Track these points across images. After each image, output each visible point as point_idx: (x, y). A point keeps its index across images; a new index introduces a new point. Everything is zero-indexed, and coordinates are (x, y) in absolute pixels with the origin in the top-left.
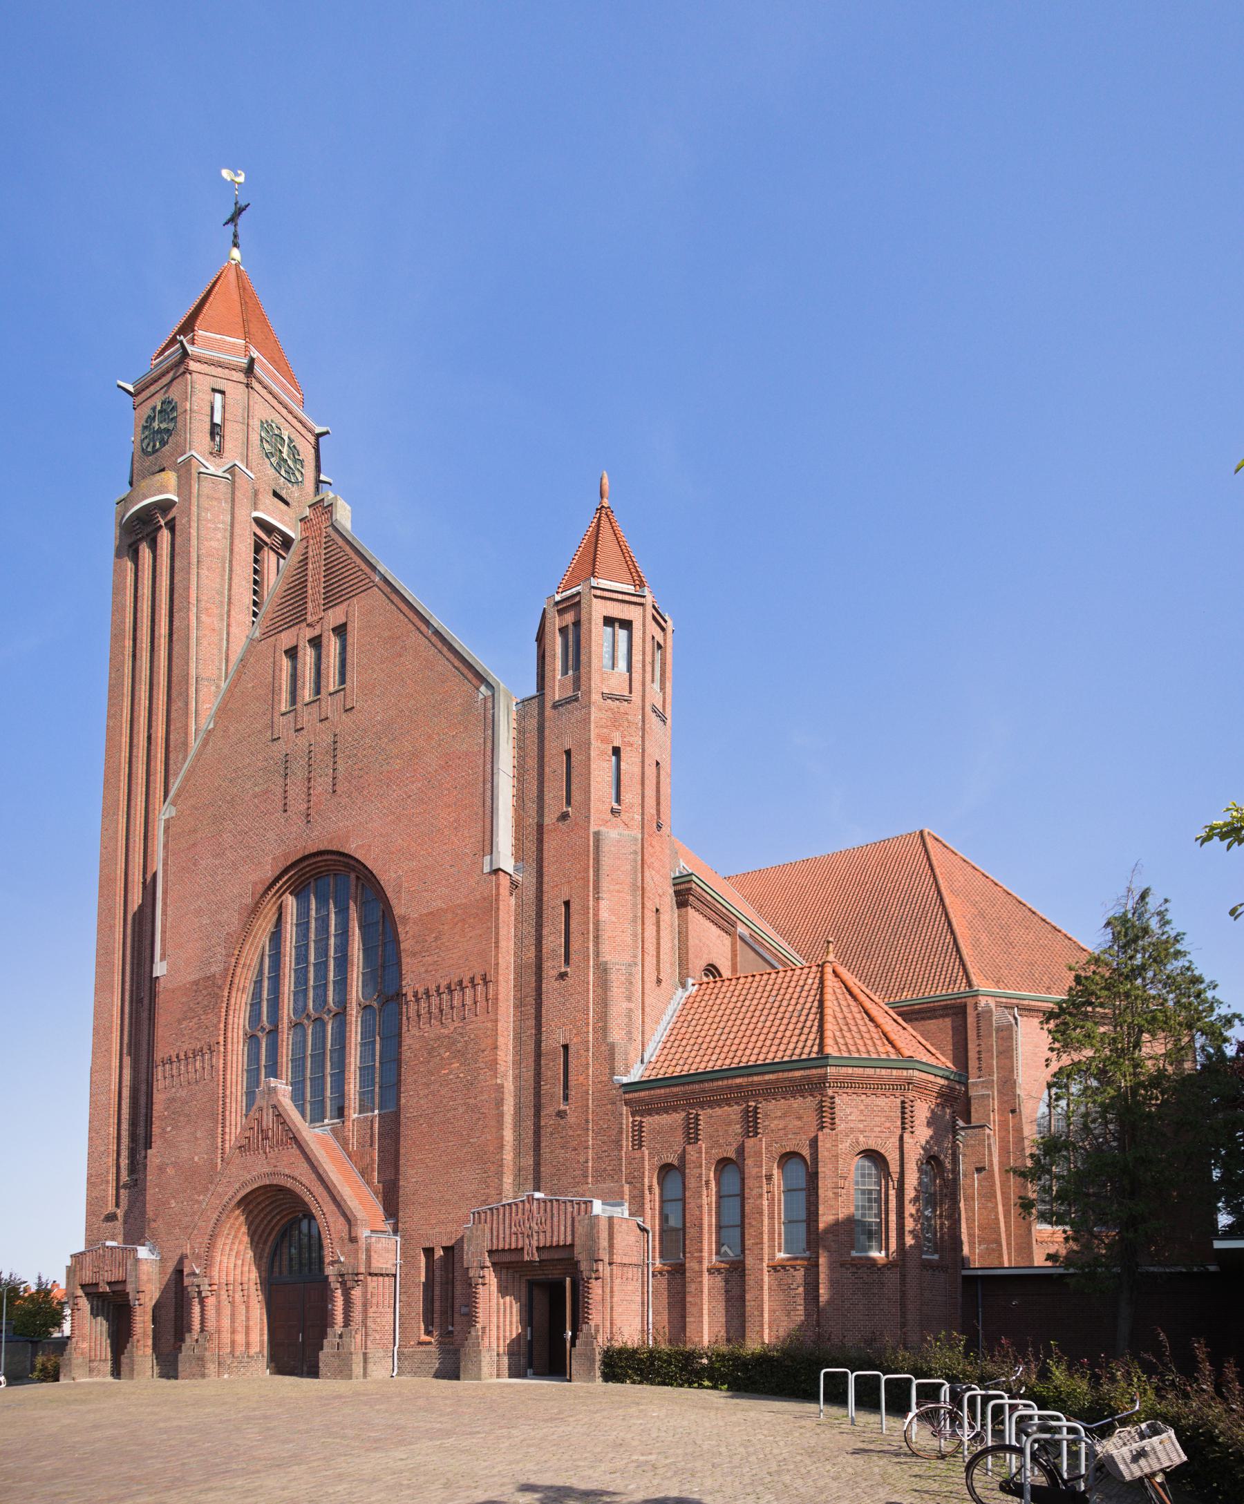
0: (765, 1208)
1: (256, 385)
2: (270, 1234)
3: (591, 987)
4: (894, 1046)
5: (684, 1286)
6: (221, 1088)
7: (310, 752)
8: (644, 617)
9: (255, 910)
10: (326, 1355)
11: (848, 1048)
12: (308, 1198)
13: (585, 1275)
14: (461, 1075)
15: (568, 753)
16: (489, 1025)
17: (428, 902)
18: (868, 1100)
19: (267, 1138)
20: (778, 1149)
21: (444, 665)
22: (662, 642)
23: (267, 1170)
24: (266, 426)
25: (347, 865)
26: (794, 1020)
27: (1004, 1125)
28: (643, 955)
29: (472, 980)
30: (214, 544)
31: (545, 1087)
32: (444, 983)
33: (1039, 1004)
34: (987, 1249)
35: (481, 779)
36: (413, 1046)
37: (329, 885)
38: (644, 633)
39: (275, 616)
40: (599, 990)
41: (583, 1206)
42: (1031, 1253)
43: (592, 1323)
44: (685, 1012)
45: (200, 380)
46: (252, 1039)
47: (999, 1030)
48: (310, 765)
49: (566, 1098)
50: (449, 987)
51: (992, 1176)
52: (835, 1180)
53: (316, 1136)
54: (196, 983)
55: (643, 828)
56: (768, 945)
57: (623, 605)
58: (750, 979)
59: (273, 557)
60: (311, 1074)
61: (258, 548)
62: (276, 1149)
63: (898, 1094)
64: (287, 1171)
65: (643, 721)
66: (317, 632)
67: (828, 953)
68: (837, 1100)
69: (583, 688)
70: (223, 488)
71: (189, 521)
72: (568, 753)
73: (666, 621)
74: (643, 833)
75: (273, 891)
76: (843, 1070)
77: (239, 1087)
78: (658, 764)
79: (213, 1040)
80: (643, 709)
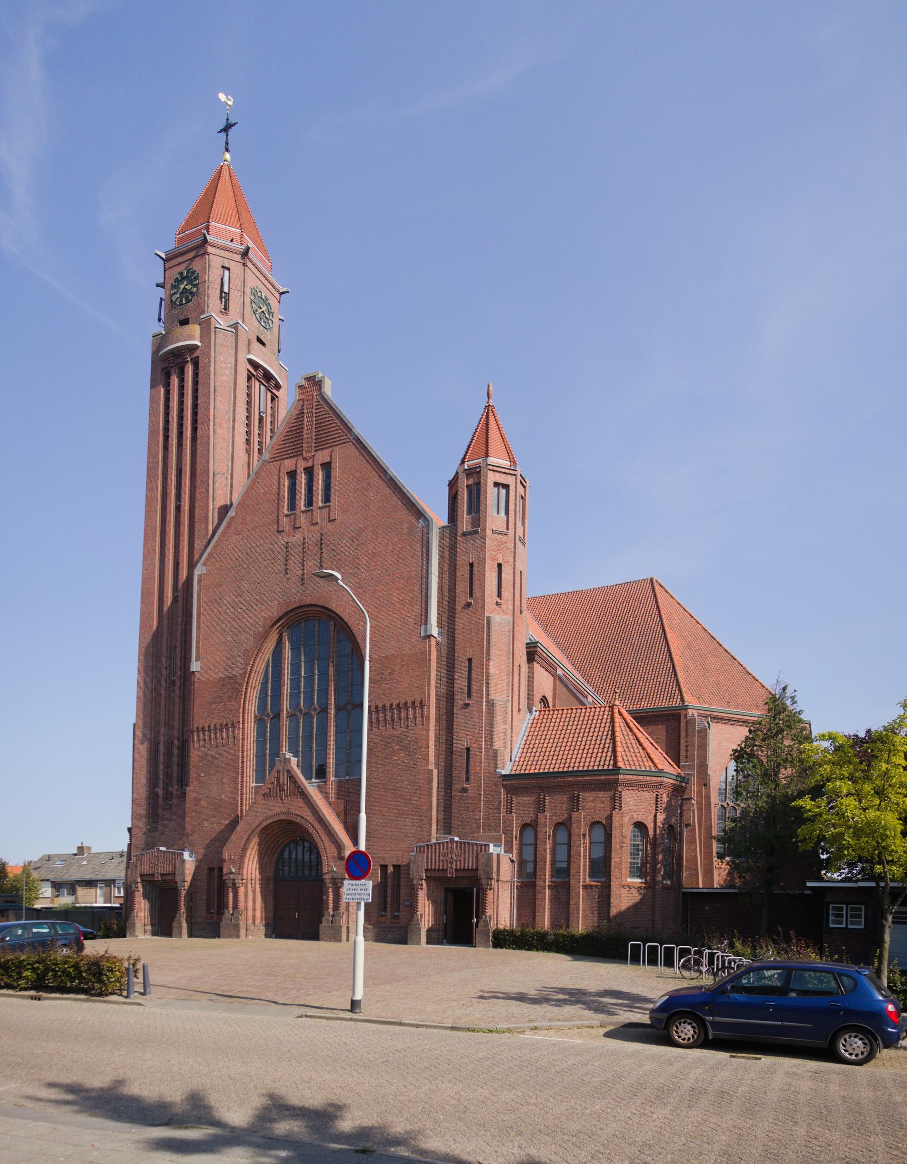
0: (582, 852)
1: (249, 264)
2: (277, 849)
3: (484, 714)
4: (653, 762)
5: (535, 894)
6: (241, 751)
7: (304, 543)
8: (516, 483)
9: (264, 637)
10: (324, 925)
11: (629, 763)
12: (311, 830)
13: (484, 886)
14: (406, 761)
15: (471, 565)
16: (424, 732)
17: (384, 649)
18: (639, 794)
19: (283, 790)
20: (590, 819)
21: (395, 501)
22: (523, 495)
23: (283, 810)
24: (254, 292)
25: (329, 616)
26: (598, 742)
27: (699, 793)
28: (512, 695)
29: (414, 703)
30: (225, 378)
31: (455, 772)
32: (395, 703)
33: (723, 715)
34: (690, 874)
35: (420, 575)
36: (375, 740)
37: (315, 626)
38: (516, 493)
39: (279, 447)
40: (489, 717)
41: (483, 847)
42: (713, 875)
43: (488, 914)
44: (533, 729)
45: (215, 260)
46: (260, 721)
47: (699, 732)
48: (304, 552)
49: (468, 779)
50: (398, 705)
51: (695, 829)
52: (621, 838)
53: (311, 788)
54: (223, 679)
55: (514, 614)
56: (571, 679)
57: (504, 475)
58: (570, 711)
59: (257, 383)
60: (302, 749)
61: (249, 379)
62: (289, 798)
63: (654, 791)
64: (297, 812)
65: (515, 548)
66: (310, 464)
67: (615, 699)
68: (623, 793)
69: (481, 526)
70: (231, 339)
71: (209, 362)
72: (471, 565)
73: (526, 482)
74: (513, 618)
75: (278, 625)
76: (628, 777)
77: (252, 752)
78: (521, 572)
79: (235, 720)
80: (515, 540)
